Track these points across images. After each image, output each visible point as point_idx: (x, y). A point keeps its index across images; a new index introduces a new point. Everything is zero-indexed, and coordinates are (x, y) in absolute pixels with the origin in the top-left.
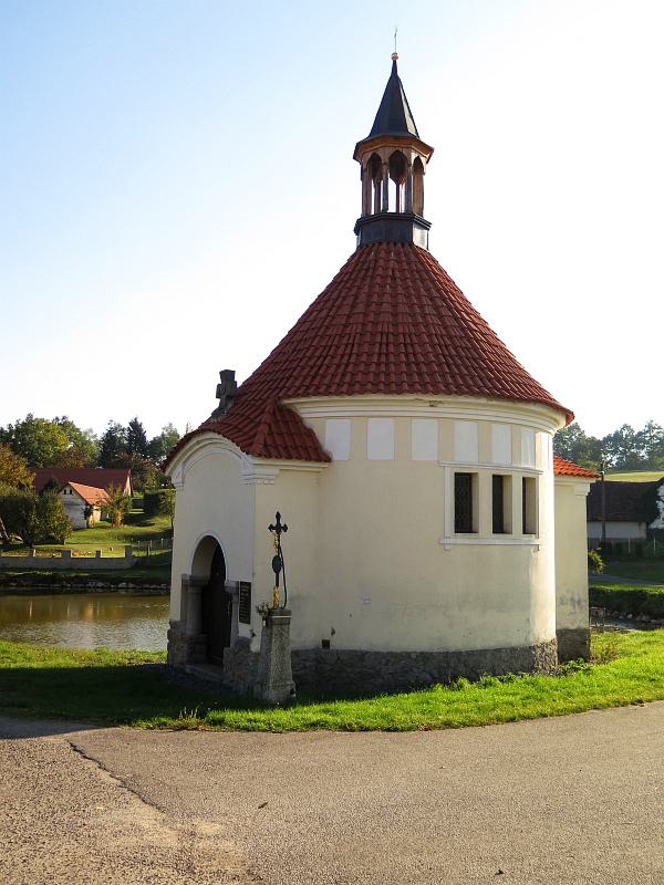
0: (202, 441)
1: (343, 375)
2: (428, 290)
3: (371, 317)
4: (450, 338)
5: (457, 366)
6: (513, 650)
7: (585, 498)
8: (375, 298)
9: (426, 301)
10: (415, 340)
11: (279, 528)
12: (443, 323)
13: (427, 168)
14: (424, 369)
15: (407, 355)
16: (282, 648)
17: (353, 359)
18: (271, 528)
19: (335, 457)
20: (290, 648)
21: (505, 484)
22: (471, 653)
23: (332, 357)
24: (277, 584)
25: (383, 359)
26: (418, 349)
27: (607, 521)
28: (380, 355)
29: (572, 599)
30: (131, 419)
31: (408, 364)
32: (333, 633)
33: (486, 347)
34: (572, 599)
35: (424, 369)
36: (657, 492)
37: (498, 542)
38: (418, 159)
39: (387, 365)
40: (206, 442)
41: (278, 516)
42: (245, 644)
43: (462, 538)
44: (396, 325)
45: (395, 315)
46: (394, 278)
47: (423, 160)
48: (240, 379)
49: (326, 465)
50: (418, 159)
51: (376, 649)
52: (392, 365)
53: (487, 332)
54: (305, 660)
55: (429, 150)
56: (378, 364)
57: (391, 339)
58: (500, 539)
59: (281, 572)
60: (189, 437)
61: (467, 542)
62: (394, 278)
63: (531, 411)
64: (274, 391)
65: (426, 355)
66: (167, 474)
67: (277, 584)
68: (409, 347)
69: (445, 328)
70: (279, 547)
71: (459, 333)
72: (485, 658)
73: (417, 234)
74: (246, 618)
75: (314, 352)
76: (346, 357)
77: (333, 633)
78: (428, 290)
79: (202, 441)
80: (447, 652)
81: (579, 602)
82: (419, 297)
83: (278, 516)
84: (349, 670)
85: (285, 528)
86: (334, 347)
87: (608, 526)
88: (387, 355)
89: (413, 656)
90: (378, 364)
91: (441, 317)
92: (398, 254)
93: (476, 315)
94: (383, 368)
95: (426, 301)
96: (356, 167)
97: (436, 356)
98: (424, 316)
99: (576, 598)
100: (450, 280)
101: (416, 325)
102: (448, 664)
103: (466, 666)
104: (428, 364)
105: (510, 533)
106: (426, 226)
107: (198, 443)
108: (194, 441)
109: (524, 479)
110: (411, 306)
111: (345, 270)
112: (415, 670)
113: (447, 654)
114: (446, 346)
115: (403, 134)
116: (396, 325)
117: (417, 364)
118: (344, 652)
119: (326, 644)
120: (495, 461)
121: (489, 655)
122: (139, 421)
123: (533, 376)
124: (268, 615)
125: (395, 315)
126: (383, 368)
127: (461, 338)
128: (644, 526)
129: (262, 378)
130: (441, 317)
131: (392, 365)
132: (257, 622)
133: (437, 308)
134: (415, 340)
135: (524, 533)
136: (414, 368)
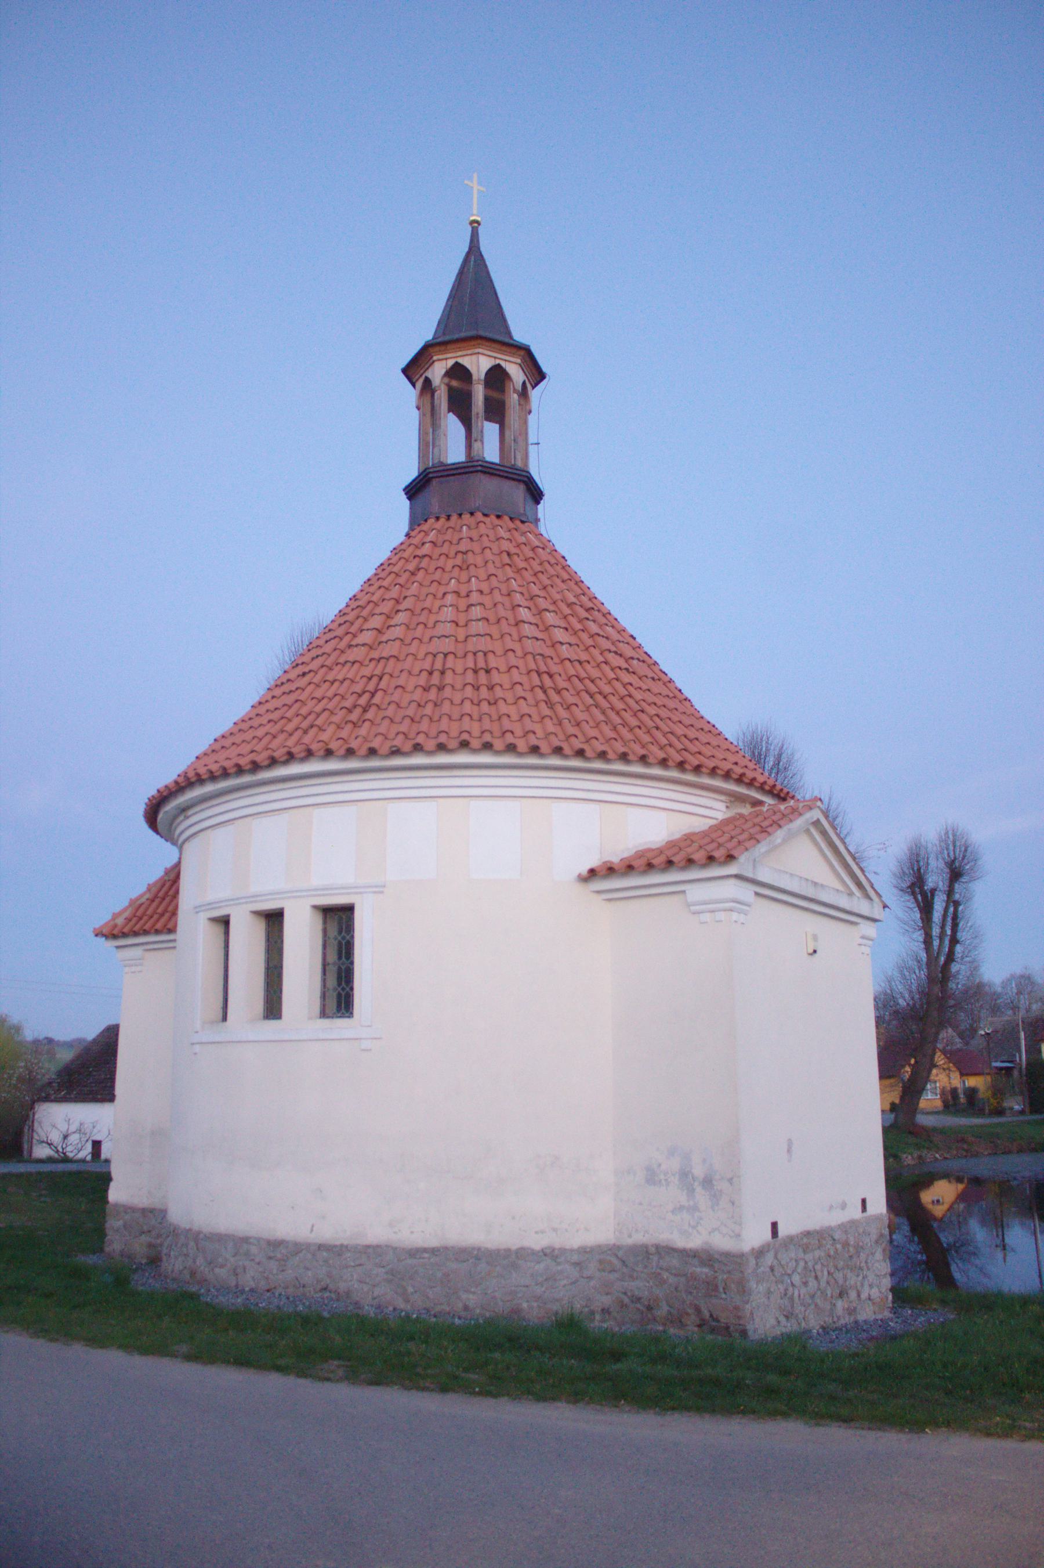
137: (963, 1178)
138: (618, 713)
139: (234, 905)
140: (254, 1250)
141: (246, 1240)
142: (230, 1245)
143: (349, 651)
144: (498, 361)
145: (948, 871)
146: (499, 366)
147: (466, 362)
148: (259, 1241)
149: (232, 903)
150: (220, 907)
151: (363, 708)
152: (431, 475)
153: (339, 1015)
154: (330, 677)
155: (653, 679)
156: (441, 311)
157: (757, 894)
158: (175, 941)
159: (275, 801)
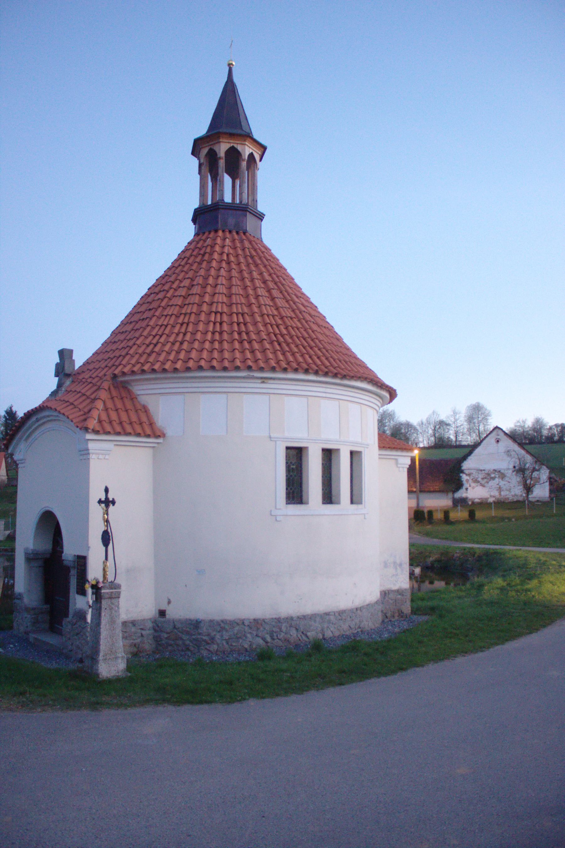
0: (41, 418)
1: (178, 352)
2: (261, 274)
3: (207, 298)
4: (282, 318)
5: (288, 345)
6: (341, 613)
7: (406, 470)
8: (211, 281)
9: (258, 283)
10: (248, 319)
11: (107, 502)
12: (275, 304)
13: (260, 165)
14: (256, 346)
15: (240, 333)
16: (112, 621)
17: (188, 337)
18: (100, 502)
19: (169, 432)
20: (119, 621)
21: (334, 457)
22: (304, 617)
23: (168, 336)
24: (107, 559)
25: (217, 336)
26: (251, 328)
27: (421, 491)
28: (213, 333)
29: (395, 563)
30: (6, 407)
31: (241, 342)
32: (169, 602)
33: (315, 327)
34: (395, 563)
35: (256, 346)
36: (461, 467)
37: (327, 512)
38: (251, 156)
39: (221, 342)
40: (45, 420)
41: (107, 490)
42: (81, 615)
43: (294, 509)
44: (230, 306)
45: (230, 296)
46: (229, 263)
47: (257, 157)
48: (79, 360)
49: (160, 440)
50: (251, 156)
51: (211, 617)
52: (225, 343)
53: (317, 314)
54: (142, 629)
55: (264, 148)
56: (212, 342)
57: (225, 318)
58: (330, 509)
59: (110, 547)
60: (29, 415)
61: (298, 513)
62: (229, 263)
63: (353, 387)
64: (110, 368)
65: (258, 333)
66: (9, 451)
67: (107, 559)
68: (242, 325)
69: (277, 309)
70: (107, 521)
71: (290, 313)
72: (315, 621)
73: (250, 221)
74: (82, 592)
75: (150, 331)
76: (181, 336)
77: (169, 602)
78: (261, 274)
79: (41, 418)
80: (280, 618)
81: (400, 565)
82: (252, 280)
83: (107, 490)
84: (185, 637)
85: (113, 502)
86: (169, 327)
87: (422, 496)
88: (221, 324)
89: (247, 623)
90: (212, 342)
91: (273, 299)
92: (233, 241)
93: (307, 299)
94: (216, 345)
95: (258, 283)
96: (195, 162)
97: (268, 334)
98: (257, 297)
99: (398, 562)
100: (281, 267)
101: (250, 305)
102: (280, 629)
103: (297, 629)
104: (261, 341)
105: (338, 503)
106: (260, 217)
107: (38, 420)
108: (34, 419)
109: (352, 453)
110: (245, 288)
111: (182, 256)
112: (249, 635)
113: (278, 620)
114: (278, 326)
115: (239, 132)
116: (230, 306)
117: (250, 342)
118: (180, 621)
119: (162, 613)
120: (324, 436)
121: (318, 619)
122: (14, 409)
123: (359, 356)
124: (96, 588)
125: (230, 296)
126: (216, 345)
127: (291, 318)
128: (450, 495)
129: (100, 357)
130: (273, 299)
131: (225, 343)
132: (90, 597)
133: (265, 282)
134: (248, 319)
135: (352, 502)
136: (246, 345)
137: (71, 658)
138: (312, 340)
139: (312, 442)
140: (332, 618)
141: (327, 614)
142: (318, 619)
143: (174, 299)
144: (232, 145)
145: (467, 424)
146: (233, 147)
147: (239, 148)
148: (335, 614)
149: (311, 441)
150: (301, 442)
151: (183, 333)
152: (220, 207)
153: (293, 502)
154: (165, 313)
155: (313, 323)
156: (212, 115)
157: (115, 445)
158: (379, 455)
159: (218, 387)
